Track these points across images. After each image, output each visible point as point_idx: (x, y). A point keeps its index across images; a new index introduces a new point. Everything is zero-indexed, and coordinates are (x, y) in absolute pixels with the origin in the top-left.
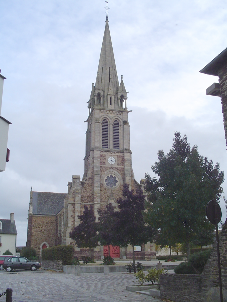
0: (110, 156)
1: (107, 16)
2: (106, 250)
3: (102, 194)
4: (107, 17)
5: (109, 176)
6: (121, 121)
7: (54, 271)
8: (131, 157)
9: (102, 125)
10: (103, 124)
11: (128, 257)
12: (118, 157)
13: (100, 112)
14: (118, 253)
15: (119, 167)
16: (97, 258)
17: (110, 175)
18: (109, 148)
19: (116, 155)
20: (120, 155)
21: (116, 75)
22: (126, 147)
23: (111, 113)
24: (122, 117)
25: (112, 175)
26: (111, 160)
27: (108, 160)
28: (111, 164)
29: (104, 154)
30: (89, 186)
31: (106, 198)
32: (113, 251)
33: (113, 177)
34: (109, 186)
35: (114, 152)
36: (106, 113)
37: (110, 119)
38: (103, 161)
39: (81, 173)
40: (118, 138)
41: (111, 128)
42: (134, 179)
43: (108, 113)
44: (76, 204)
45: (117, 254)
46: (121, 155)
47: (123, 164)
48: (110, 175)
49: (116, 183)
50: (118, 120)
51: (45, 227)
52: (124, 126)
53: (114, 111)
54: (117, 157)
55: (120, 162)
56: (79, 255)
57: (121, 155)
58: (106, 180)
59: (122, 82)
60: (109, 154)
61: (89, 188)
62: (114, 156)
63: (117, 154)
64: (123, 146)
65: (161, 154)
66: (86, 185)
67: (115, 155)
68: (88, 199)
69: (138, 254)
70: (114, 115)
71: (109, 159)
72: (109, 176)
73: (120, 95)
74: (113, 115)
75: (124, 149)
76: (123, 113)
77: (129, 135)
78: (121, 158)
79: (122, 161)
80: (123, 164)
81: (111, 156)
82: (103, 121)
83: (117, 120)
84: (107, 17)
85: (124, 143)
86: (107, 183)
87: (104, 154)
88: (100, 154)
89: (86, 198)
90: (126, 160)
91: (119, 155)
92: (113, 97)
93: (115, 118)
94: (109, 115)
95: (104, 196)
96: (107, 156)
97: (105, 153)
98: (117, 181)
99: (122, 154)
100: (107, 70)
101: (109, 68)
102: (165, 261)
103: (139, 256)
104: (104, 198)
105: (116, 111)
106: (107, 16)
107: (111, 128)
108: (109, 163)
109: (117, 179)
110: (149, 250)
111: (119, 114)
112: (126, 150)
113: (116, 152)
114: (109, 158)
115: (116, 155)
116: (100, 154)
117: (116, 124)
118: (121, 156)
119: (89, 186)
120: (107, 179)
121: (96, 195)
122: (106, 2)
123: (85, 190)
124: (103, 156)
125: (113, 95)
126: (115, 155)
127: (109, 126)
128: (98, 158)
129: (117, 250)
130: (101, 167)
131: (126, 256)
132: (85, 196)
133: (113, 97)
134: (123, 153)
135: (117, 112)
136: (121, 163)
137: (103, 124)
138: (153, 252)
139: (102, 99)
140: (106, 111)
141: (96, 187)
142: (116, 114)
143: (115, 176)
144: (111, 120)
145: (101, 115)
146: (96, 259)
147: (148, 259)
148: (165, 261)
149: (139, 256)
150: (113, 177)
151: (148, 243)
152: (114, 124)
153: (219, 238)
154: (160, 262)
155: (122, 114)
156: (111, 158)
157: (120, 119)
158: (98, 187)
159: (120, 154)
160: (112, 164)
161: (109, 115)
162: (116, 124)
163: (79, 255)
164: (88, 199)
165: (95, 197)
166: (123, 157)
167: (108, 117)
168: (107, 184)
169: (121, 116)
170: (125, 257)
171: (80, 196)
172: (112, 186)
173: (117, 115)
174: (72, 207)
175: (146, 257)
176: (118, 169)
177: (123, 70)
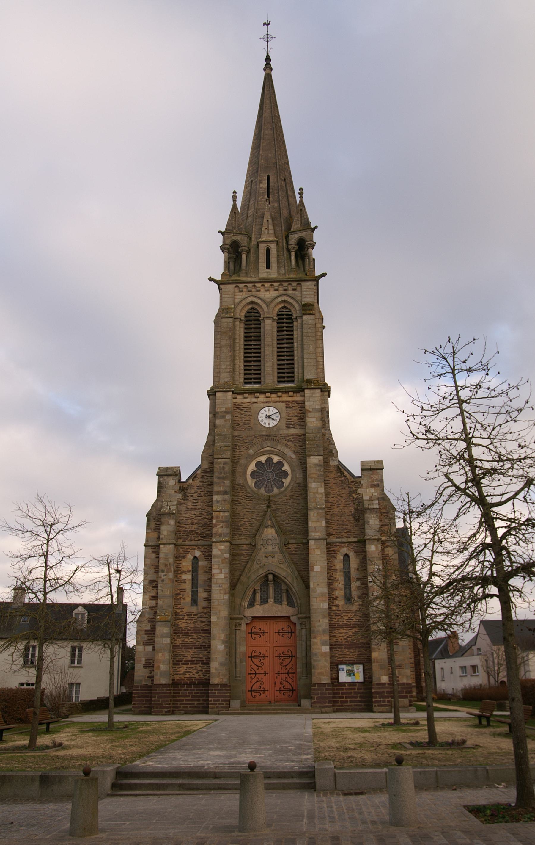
0: (262, 405)
4: (268, 59)
5: (276, 459)
6: (296, 305)
9: (246, 325)
10: (247, 321)
11: (315, 703)
13: (237, 291)
14: (293, 690)
15: (292, 431)
16: (217, 707)
18: (262, 383)
19: (281, 399)
21: (290, 193)
23: (266, 289)
24: (300, 295)
27: (260, 415)
28: (267, 425)
29: (248, 400)
31: (251, 524)
32: (278, 681)
34: (262, 491)
35: (254, 393)
37: (264, 306)
41: (269, 327)
42: (336, 463)
43: (259, 291)
45: (290, 690)
46: (298, 398)
47: (302, 424)
49: (284, 480)
52: (305, 317)
53: (274, 282)
55: (295, 420)
56: (165, 697)
59: (301, 202)
60: (262, 398)
61: (204, 498)
62: (278, 404)
63: (285, 397)
64: (303, 373)
66: (193, 491)
67: (278, 399)
69: (355, 693)
70: (276, 293)
71: (263, 414)
73: (294, 238)
74: (273, 294)
75: (303, 380)
76: (302, 283)
77: (320, 342)
78: (297, 408)
80: (302, 424)
83: (286, 305)
84: (268, 59)
85: (305, 364)
86: (255, 480)
87: (248, 400)
88: (235, 400)
89: (194, 527)
91: (290, 399)
92: (273, 247)
93: (280, 299)
94: (263, 294)
95: (246, 520)
96: (254, 405)
97: (251, 399)
98: (285, 474)
99: (298, 395)
100: (261, 182)
103: (351, 701)
105: (281, 281)
107: (269, 327)
110: (385, 679)
111: (290, 288)
112: (309, 381)
113: (283, 392)
114: (262, 411)
115: (281, 399)
116: (235, 400)
117: (285, 320)
120: (255, 469)
122: (265, 24)
123: (190, 506)
124: (244, 406)
125: (273, 241)
127: (262, 324)
128: (227, 413)
130: (234, 437)
132: (190, 521)
133: (273, 247)
135: (285, 284)
136: (297, 421)
137: (247, 321)
138: (404, 684)
139: (244, 256)
140: (254, 286)
141: (218, 493)
142: (281, 289)
144: (268, 306)
145: (239, 296)
147: (381, 709)
149: (351, 701)
151: (434, 632)
152: (279, 319)
155: (298, 288)
156: (267, 409)
157: (294, 303)
158: (225, 493)
160: (272, 425)
161: (263, 294)
162: (285, 320)
163: (165, 697)
165: (214, 522)
167: (259, 301)
168: (256, 483)
169: (297, 293)
171: (172, 522)
172: (273, 490)
173: (284, 292)
174: (153, 552)
175: (376, 702)
176: (288, 438)
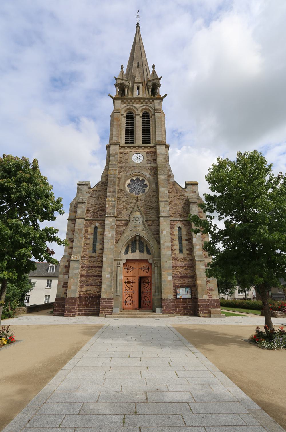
2: (128, 296)
3: (122, 205)
4: (138, 24)
5: (134, 178)
7: (246, 347)
8: (167, 152)
11: (164, 310)
12: (148, 153)
16: (105, 312)
17: (136, 177)
20: (150, 150)
22: (159, 139)
25: (139, 177)
26: (138, 158)
28: (136, 162)
30: (101, 194)
31: (127, 209)
33: (140, 179)
36: (131, 103)
38: (125, 159)
39: (95, 179)
40: (149, 132)
41: (139, 122)
42: (173, 181)
44: (77, 220)
46: (153, 150)
48: (136, 177)
50: (148, 111)
57: (153, 150)
58: (129, 185)
65: (227, 159)
71: (134, 157)
72: (134, 178)
79: (153, 156)
80: (155, 162)
81: (137, 152)
82: (128, 114)
83: (146, 111)
84: (138, 24)
90: (160, 154)
92: (141, 85)
97: (128, 150)
98: (146, 186)
99: (153, 148)
101: (138, 62)
102: (53, 253)
104: (125, 209)
107: (139, 122)
109: (146, 182)
110: (205, 297)
117: (146, 118)
118: (151, 151)
119: (101, 194)
120: (130, 183)
121: (109, 204)
124: (125, 153)
129: (128, 289)
131: (162, 307)
134: (155, 148)
142: (144, 103)
143: (144, 179)
146: (102, 313)
148: (53, 253)
150: (140, 179)
159: (151, 148)
162: (146, 118)
165: (107, 206)
167: (133, 108)
170: (158, 310)
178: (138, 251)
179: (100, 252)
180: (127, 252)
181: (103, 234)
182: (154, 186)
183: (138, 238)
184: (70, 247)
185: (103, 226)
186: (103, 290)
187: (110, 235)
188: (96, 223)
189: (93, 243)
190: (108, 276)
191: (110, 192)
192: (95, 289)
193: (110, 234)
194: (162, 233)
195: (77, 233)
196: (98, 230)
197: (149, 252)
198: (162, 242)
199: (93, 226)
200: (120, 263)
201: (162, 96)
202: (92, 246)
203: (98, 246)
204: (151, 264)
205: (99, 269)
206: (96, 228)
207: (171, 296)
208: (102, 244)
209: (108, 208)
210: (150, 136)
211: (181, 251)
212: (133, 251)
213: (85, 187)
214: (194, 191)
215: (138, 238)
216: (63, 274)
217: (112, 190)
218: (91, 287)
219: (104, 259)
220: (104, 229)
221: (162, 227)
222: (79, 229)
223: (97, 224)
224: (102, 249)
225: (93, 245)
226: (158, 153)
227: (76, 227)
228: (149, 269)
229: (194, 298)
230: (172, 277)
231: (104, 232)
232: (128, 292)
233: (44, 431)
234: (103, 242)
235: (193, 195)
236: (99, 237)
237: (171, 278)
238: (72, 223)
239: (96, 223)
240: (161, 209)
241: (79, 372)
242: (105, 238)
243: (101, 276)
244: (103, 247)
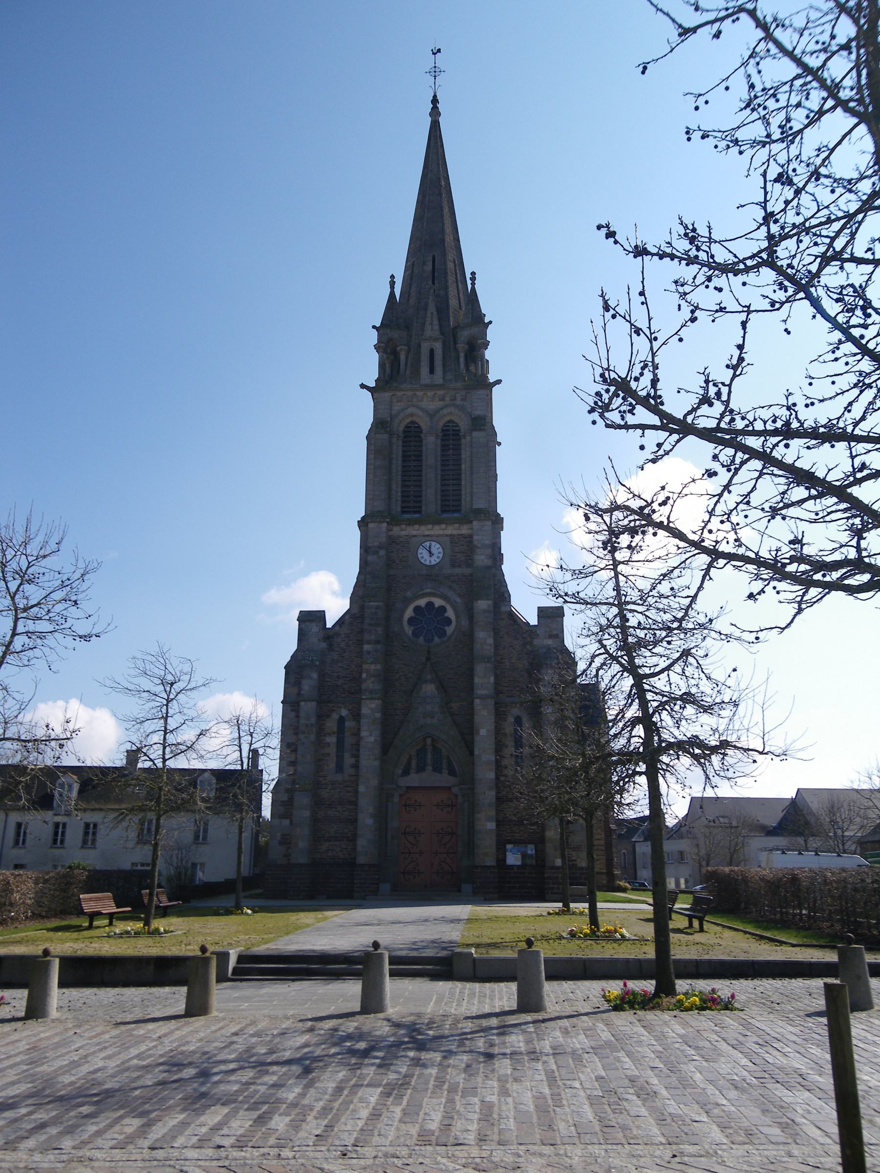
1: (435, 96)
4: (435, 101)
15: (458, 571)
20: (459, 532)
22: (480, 504)
51: (453, 1089)
54: (447, 539)
68: (345, 686)
81: (427, 538)
84: (435, 101)
90: (479, 545)
91: (455, 532)
106: (435, 96)
108: (422, 561)
116: (390, 533)
126: (441, 532)
153: (826, 80)
154: (625, 985)
162: (451, 436)
164: (345, 686)
165: (364, 676)
166: (471, 536)
171: (315, 676)
177: (438, 97)
178: (431, 768)
179: (352, 771)
180: (406, 772)
181: (357, 733)
182: (465, 622)
183: (429, 741)
184: (291, 762)
185: (357, 716)
186: (359, 849)
187: (372, 739)
188: (343, 710)
189: (337, 752)
190: (369, 821)
191: (369, 643)
192: (344, 846)
193: (371, 735)
194: (478, 734)
195: (303, 733)
196: (348, 724)
197: (452, 772)
198: (476, 752)
199: (335, 716)
200: (462, 400)
201: (491, 381)
202: (335, 758)
203: (349, 760)
204: (456, 796)
205: (350, 807)
206: (342, 720)
207: (490, 861)
208: (356, 756)
209: (365, 680)
210: (460, 490)
211: (339, 768)
212: (421, 769)
213: (315, 628)
214: (555, 632)
215: (429, 741)
216: (279, 818)
217: (373, 637)
218: (337, 843)
219: (362, 789)
220: (359, 722)
221: (477, 719)
222: (307, 726)
223: (344, 712)
224: (356, 766)
225: (337, 756)
226: (475, 543)
227: (302, 721)
228: (453, 806)
229: (540, 862)
230: (494, 824)
231: (359, 729)
232: (410, 853)
233: (238, 1123)
234: (358, 750)
235: (549, 642)
236: (349, 740)
237: (491, 825)
238: (293, 711)
239: (343, 710)
240: (477, 680)
241: (796, 1152)
242: (362, 744)
243: (356, 821)
244: (358, 761)
